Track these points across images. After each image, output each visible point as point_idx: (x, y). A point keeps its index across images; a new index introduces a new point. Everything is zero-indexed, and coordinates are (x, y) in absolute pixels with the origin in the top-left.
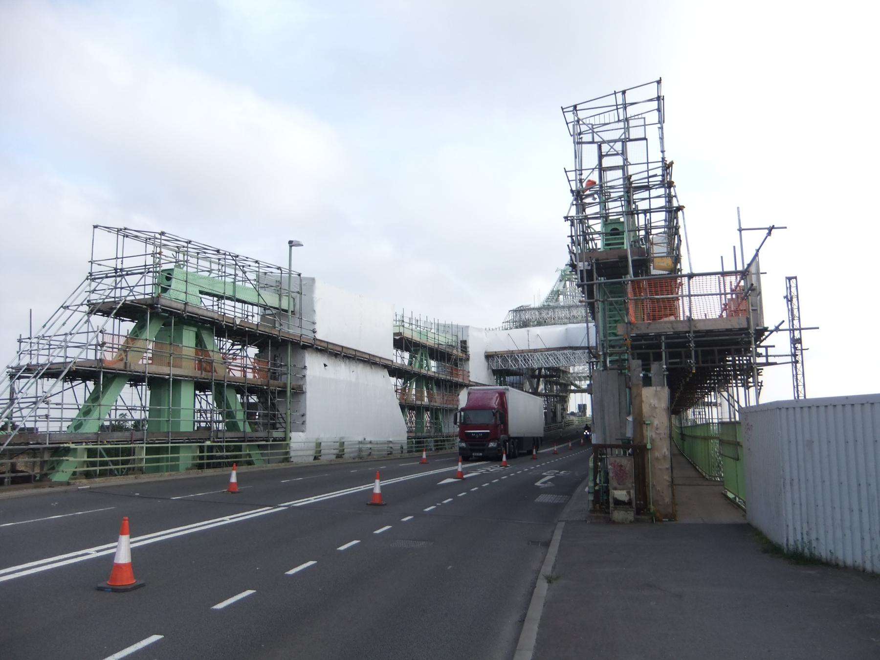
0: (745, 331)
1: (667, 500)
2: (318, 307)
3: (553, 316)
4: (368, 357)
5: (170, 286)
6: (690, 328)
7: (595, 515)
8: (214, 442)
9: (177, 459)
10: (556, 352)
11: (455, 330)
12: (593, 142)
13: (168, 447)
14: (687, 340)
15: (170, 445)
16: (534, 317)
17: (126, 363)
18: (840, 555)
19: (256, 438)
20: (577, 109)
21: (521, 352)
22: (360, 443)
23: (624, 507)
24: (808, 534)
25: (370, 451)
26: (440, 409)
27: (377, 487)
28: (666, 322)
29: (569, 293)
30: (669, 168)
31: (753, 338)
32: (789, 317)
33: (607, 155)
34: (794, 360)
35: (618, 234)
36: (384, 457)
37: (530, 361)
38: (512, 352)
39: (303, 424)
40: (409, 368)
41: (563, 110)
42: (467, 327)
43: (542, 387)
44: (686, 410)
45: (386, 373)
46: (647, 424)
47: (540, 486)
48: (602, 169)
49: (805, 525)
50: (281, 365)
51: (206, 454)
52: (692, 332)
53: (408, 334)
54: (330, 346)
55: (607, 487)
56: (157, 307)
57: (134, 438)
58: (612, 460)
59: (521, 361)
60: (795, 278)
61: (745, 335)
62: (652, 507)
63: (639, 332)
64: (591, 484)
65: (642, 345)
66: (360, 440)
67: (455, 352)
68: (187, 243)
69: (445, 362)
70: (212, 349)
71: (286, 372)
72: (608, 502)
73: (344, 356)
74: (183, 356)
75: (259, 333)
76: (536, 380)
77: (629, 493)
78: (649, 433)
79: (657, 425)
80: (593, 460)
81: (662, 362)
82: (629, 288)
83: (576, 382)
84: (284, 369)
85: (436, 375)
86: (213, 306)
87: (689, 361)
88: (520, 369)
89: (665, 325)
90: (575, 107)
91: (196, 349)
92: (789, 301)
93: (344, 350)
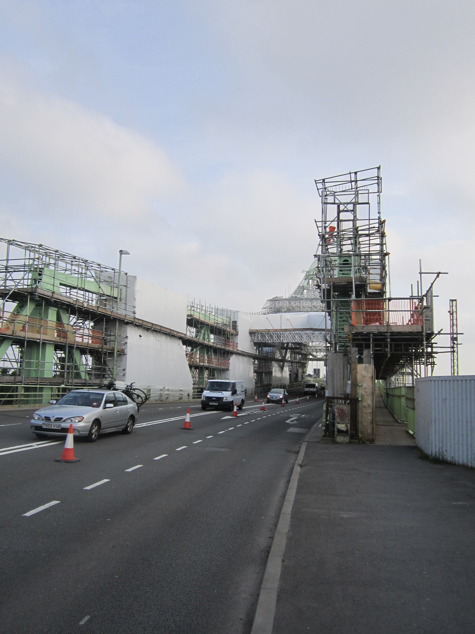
0: (420, 333)
1: (369, 431)
2: (137, 297)
3: (299, 305)
4: (160, 329)
5: (41, 279)
6: (388, 330)
7: (326, 438)
8: (66, 385)
9: (41, 396)
10: (301, 332)
11: (229, 313)
12: (334, 203)
13: (37, 387)
14: (385, 337)
15: (38, 386)
16: (285, 306)
17: (13, 331)
18: (457, 459)
19: (93, 384)
20: (325, 181)
21: (275, 330)
22: (161, 390)
23: (343, 434)
24: (442, 448)
25: (167, 396)
26: (216, 369)
27: (188, 418)
28: (373, 326)
29: (311, 289)
30: (382, 224)
31: (425, 338)
32: (451, 324)
33: (343, 211)
34: (452, 351)
35: (348, 264)
36: (177, 401)
37: (282, 338)
38: (269, 330)
39: (123, 376)
40: (196, 340)
41: (315, 182)
42: (238, 311)
43: (288, 355)
44: (390, 377)
45: (180, 342)
46: (359, 386)
47: (289, 423)
48: (339, 221)
49: (441, 444)
50: (110, 335)
51: (61, 393)
52: (389, 333)
53: (196, 316)
54: (144, 323)
55: (334, 423)
56: (35, 295)
57: (17, 380)
58: (338, 406)
59: (275, 337)
60: (456, 300)
61: (421, 336)
62: (360, 435)
63: (357, 331)
64: (324, 420)
65: (359, 338)
66: (161, 388)
67: (228, 329)
68: (55, 251)
69: (221, 336)
70: (67, 323)
71: (114, 340)
72: (334, 431)
73: (154, 330)
74: (48, 327)
75: (99, 313)
76: (285, 350)
77: (346, 426)
78: (360, 391)
79: (365, 387)
80: (325, 406)
81: (370, 350)
82: (353, 305)
83: (313, 353)
84: (112, 338)
85: (215, 345)
86: (66, 293)
87: (386, 350)
88: (273, 342)
89: (374, 327)
90: (324, 180)
91: (56, 322)
92: (451, 314)
93: (154, 326)
